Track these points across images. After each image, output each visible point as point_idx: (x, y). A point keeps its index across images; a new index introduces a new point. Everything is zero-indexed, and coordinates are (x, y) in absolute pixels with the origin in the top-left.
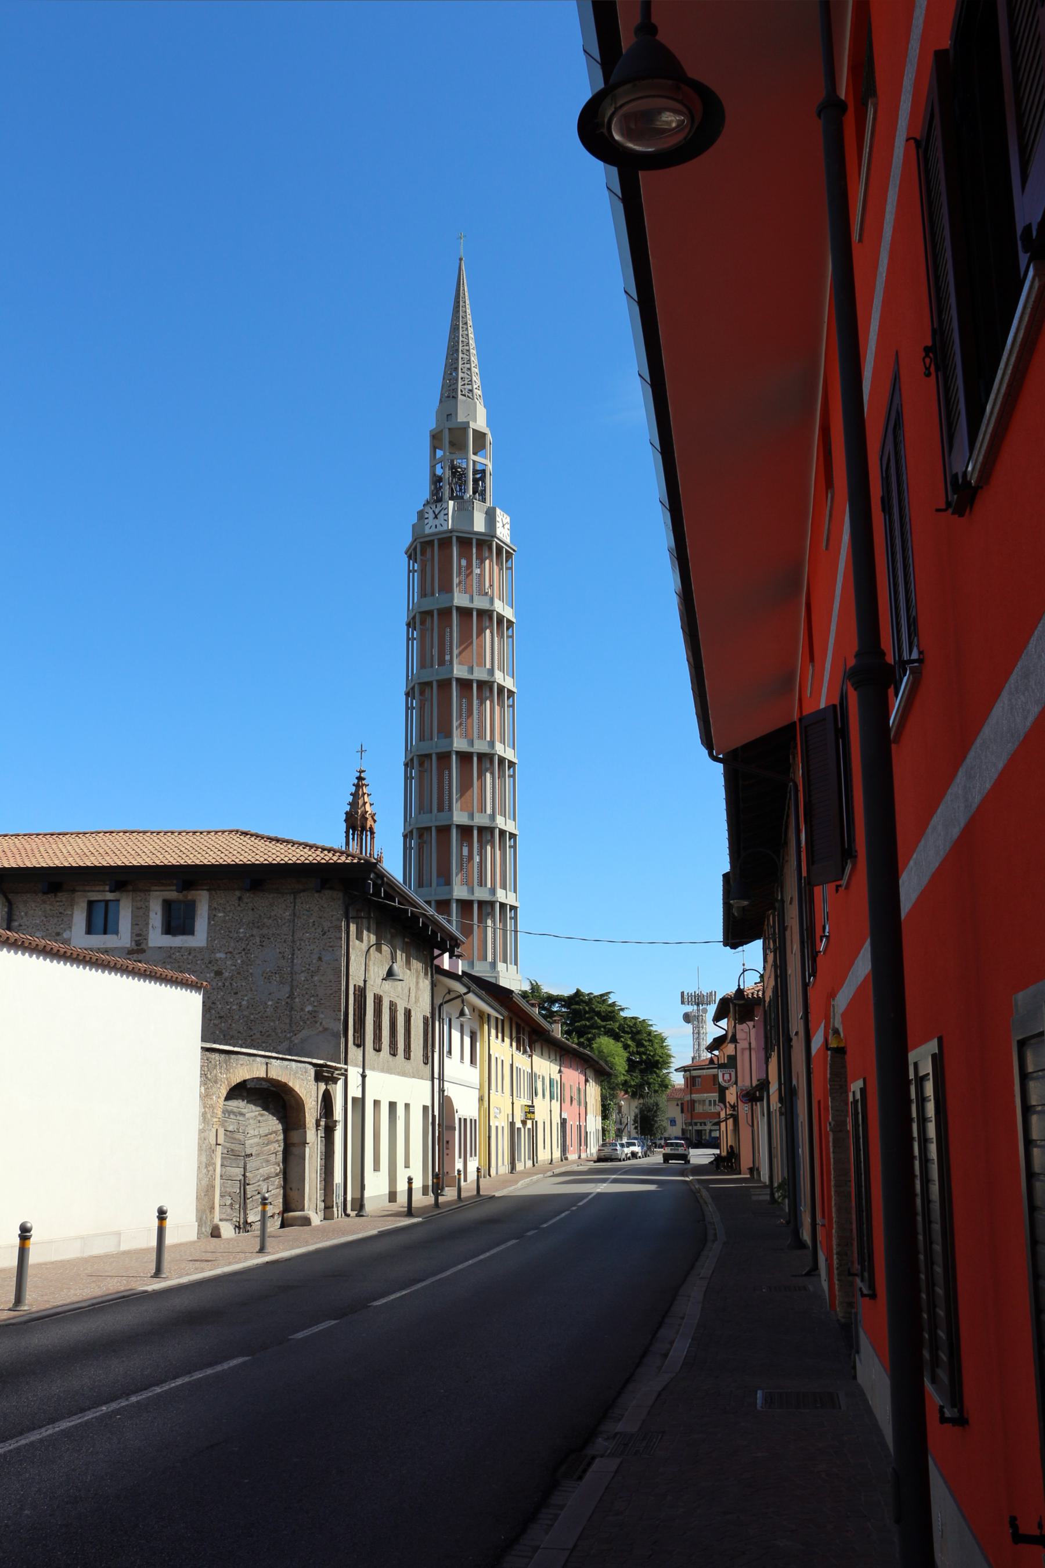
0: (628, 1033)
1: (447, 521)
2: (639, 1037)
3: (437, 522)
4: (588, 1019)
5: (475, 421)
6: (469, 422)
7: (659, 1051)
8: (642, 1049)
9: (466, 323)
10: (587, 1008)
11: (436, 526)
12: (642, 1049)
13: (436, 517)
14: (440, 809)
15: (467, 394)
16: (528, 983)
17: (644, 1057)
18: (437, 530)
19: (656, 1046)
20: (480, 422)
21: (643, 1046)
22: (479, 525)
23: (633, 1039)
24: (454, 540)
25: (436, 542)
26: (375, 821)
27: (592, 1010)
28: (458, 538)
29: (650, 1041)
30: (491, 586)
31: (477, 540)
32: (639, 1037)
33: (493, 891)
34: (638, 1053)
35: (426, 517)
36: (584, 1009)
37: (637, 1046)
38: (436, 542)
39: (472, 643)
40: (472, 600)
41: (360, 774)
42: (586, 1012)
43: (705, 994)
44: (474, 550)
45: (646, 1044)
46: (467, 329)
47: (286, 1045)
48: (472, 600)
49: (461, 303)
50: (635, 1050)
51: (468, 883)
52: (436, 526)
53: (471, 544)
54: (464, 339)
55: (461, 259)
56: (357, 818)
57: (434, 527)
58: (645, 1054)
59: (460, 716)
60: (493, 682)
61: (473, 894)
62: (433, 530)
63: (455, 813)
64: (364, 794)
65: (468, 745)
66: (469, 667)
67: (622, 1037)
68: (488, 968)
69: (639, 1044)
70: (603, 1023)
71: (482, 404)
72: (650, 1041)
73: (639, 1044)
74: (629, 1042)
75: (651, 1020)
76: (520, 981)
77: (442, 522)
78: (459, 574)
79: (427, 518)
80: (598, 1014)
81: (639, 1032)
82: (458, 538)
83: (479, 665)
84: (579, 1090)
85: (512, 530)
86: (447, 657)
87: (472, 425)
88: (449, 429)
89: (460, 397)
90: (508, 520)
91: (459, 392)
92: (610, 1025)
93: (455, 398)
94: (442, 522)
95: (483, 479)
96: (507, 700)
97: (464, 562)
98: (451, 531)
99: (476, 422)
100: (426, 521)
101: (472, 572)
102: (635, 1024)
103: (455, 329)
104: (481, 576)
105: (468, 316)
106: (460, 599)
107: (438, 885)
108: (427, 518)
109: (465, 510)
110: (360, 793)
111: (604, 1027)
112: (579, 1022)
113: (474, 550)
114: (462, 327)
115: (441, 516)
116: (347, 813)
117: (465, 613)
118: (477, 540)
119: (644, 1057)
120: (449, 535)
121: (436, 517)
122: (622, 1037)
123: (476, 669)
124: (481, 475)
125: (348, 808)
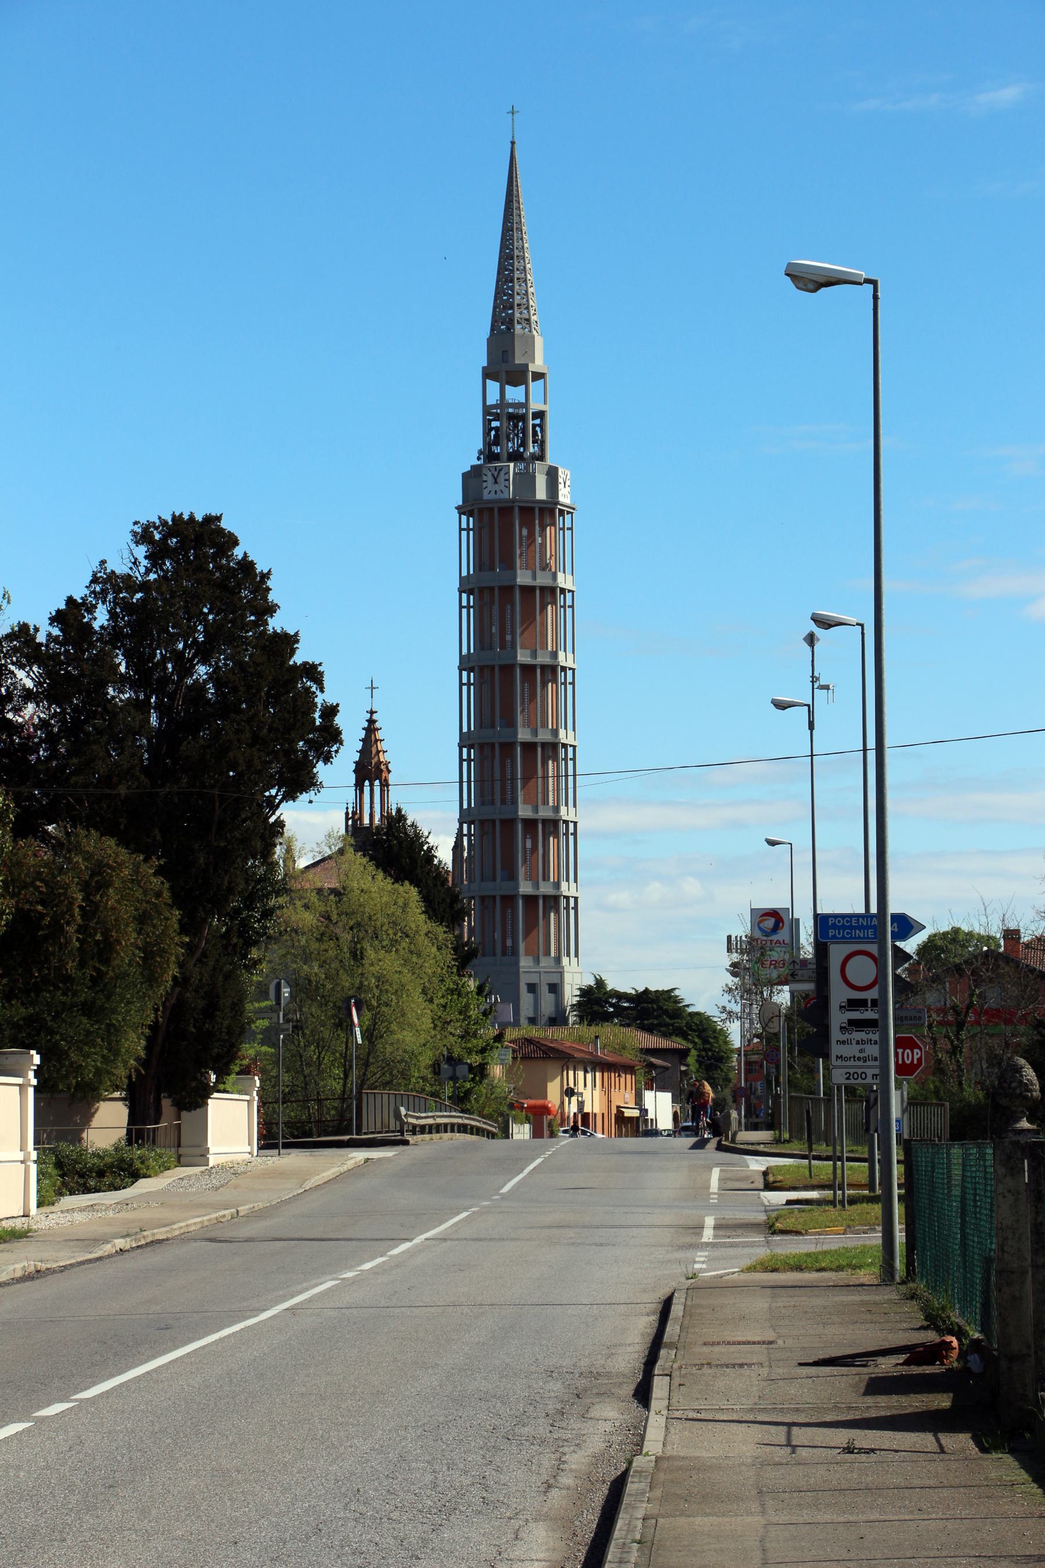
0: (694, 1031)
2: (704, 1034)
3: (497, 487)
4: (656, 1018)
6: (527, 365)
7: (724, 1048)
8: (708, 1046)
10: (655, 1006)
11: (496, 492)
12: (708, 1046)
13: (496, 482)
14: (503, 802)
16: (593, 978)
17: (710, 1054)
18: (497, 497)
19: (721, 1042)
21: (708, 1042)
23: (699, 1036)
26: (389, 771)
27: (660, 1008)
29: (715, 1038)
32: (704, 1034)
33: (557, 885)
34: (704, 1050)
35: (484, 486)
36: (653, 1007)
37: (703, 1043)
40: (534, 578)
41: (371, 716)
42: (654, 1010)
43: (735, 1020)
44: (537, 522)
45: (711, 1040)
47: (897, 1023)
48: (534, 578)
50: (701, 1047)
51: (532, 877)
52: (496, 492)
56: (371, 770)
57: (493, 493)
58: (710, 1050)
59: (523, 703)
60: (557, 666)
61: (538, 889)
62: (492, 496)
63: (520, 806)
64: (378, 752)
65: (532, 735)
66: (532, 652)
67: (689, 1035)
68: (552, 963)
69: (705, 1041)
70: (671, 1022)
72: (715, 1038)
73: (705, 1041)
74: (696, 1040)
75: (9, 602)
76: (581, 973)
77: (503, 488)
78: (521, 545)
79: (486, 481)
80: (666, 1012)
81: (704, 1030)
83: (542, 648)
86: (508, 638)
88: (507, 372)
92: (678, 1023)
94: (503, 488)
96: (540, 613)
97: (525, 532)
98: (513, 501)
99: (534, 362)
100: (485, 484)
101: (534, 540)
102: (701, 1022)
104: (543, 545)
106: (523, 578)
107: (502, 880)
108: (486, 481)
110: (374, 751)
111: (672, 1025)
112: (648, 1020)
113: (537, 522)
117: (528, 591)
119: (710, 1054)
120: (510, 504)
122: (689, 1035)
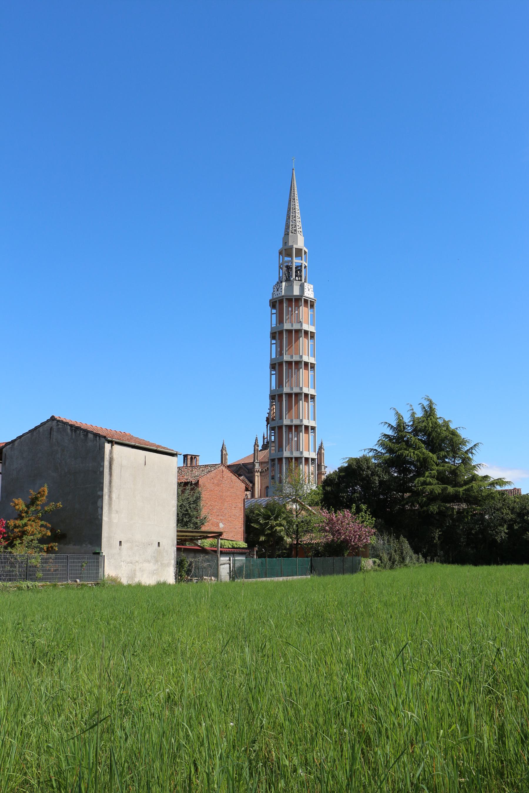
1: (282, 292)
3: (278, 293)
5: (297, 244)
6: (293, 245)
9: (294, 199)
13: (278, 291)
15: (294, 232)
20: (300, 242)
22: (296, 292)
24: (284, 300)
25: (278, 301)
28: (287, 299)
30: (302, 319)
31: (295, 299)
38: (278, 301)
39: (292, 345)
44: (294, 304)
46: (295, 202)
48: (292, 326)
49: (292, 194)
53: (292, 300)
54: (293, 215)
55: (293, 169)
62: (277, 296)
71: (302, 235)
82: (287, 299)
84: (370, 652)
85: (315, 291)
87: (295, 246)
89: (290, 234)
90: (312, 286)
91: (290, 232)
93: (288, 234)
95: (301, 271)
98: (283, 296)
103: (292, 183)
104: (299, 314)
105: (296, 195)
109: (290, 287)
113: (294, 304)
114: (292, 216)
115: (280, 290)
116: (267, 418)
118: (295, 299)
121: (278, 291)
123: (294, 356)
124: (299, 269)
125: (267, 415)
